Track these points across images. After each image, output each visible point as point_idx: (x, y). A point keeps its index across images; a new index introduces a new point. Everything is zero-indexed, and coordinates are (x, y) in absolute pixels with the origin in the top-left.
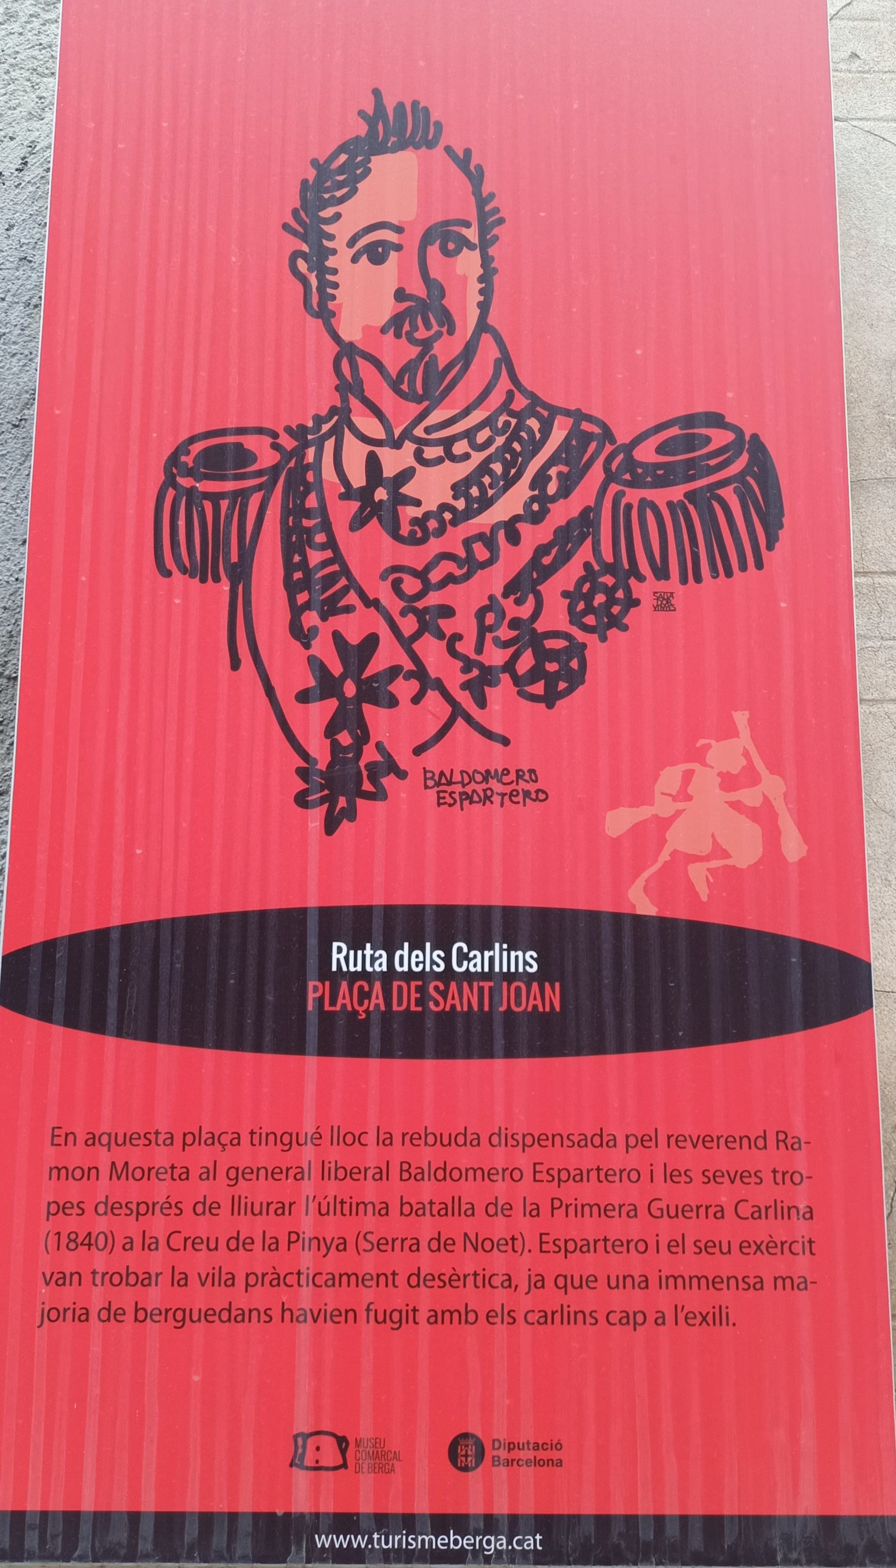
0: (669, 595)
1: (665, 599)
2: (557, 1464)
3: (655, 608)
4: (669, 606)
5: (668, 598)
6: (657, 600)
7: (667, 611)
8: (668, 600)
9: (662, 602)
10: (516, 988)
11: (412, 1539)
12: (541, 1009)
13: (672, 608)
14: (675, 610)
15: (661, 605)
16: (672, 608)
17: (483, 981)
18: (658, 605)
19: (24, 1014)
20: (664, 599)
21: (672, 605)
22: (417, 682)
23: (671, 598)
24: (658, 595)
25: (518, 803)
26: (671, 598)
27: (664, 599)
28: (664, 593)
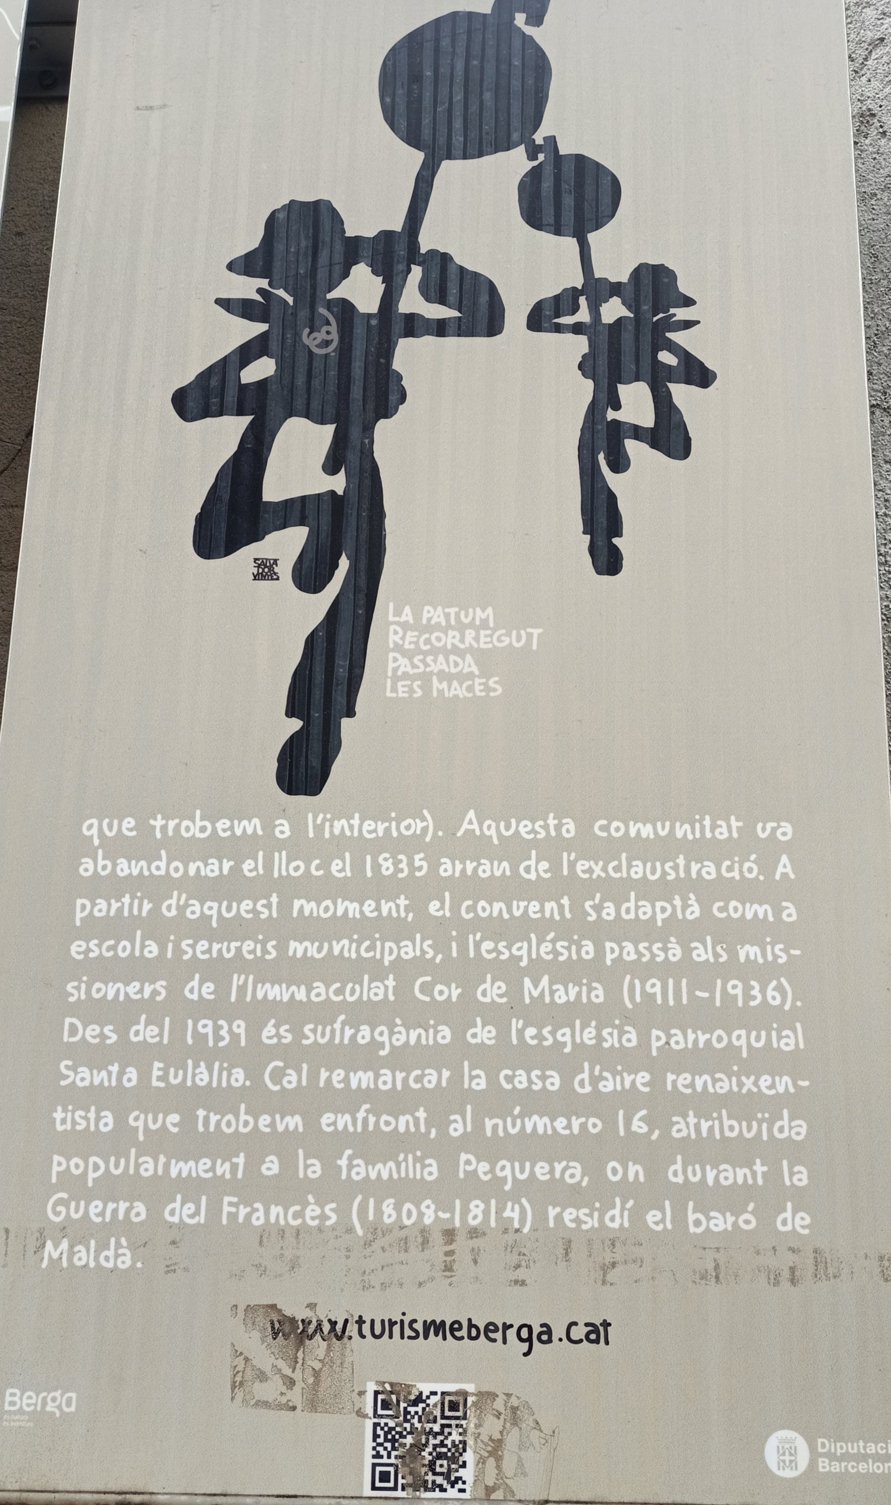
0: (272, 562)
1: (267, 567)
2: (540, 1335)
3: (255, 577)
4: (271, 574)
5: (271, 566)
6: (259, 567)
7: (268, 580)
8: (271, 568)
9: (263, 570)
10: (409, 830)
11: (67, 1067)
12: (106, 1084)
13: (275, 577)
14: (278, 579)
15: (262, 573)
16: (275, 577)
17: (448, 607)
18: (258, 574)
19: (560, 235)
20: (266, 566)
21: (275, 574)
22: (658, 356)
23: (274, 566)
24: (259, 562)
25: (462, 1338)
26: (274, 566)
27: (266, 566)
28: (267, 559)
